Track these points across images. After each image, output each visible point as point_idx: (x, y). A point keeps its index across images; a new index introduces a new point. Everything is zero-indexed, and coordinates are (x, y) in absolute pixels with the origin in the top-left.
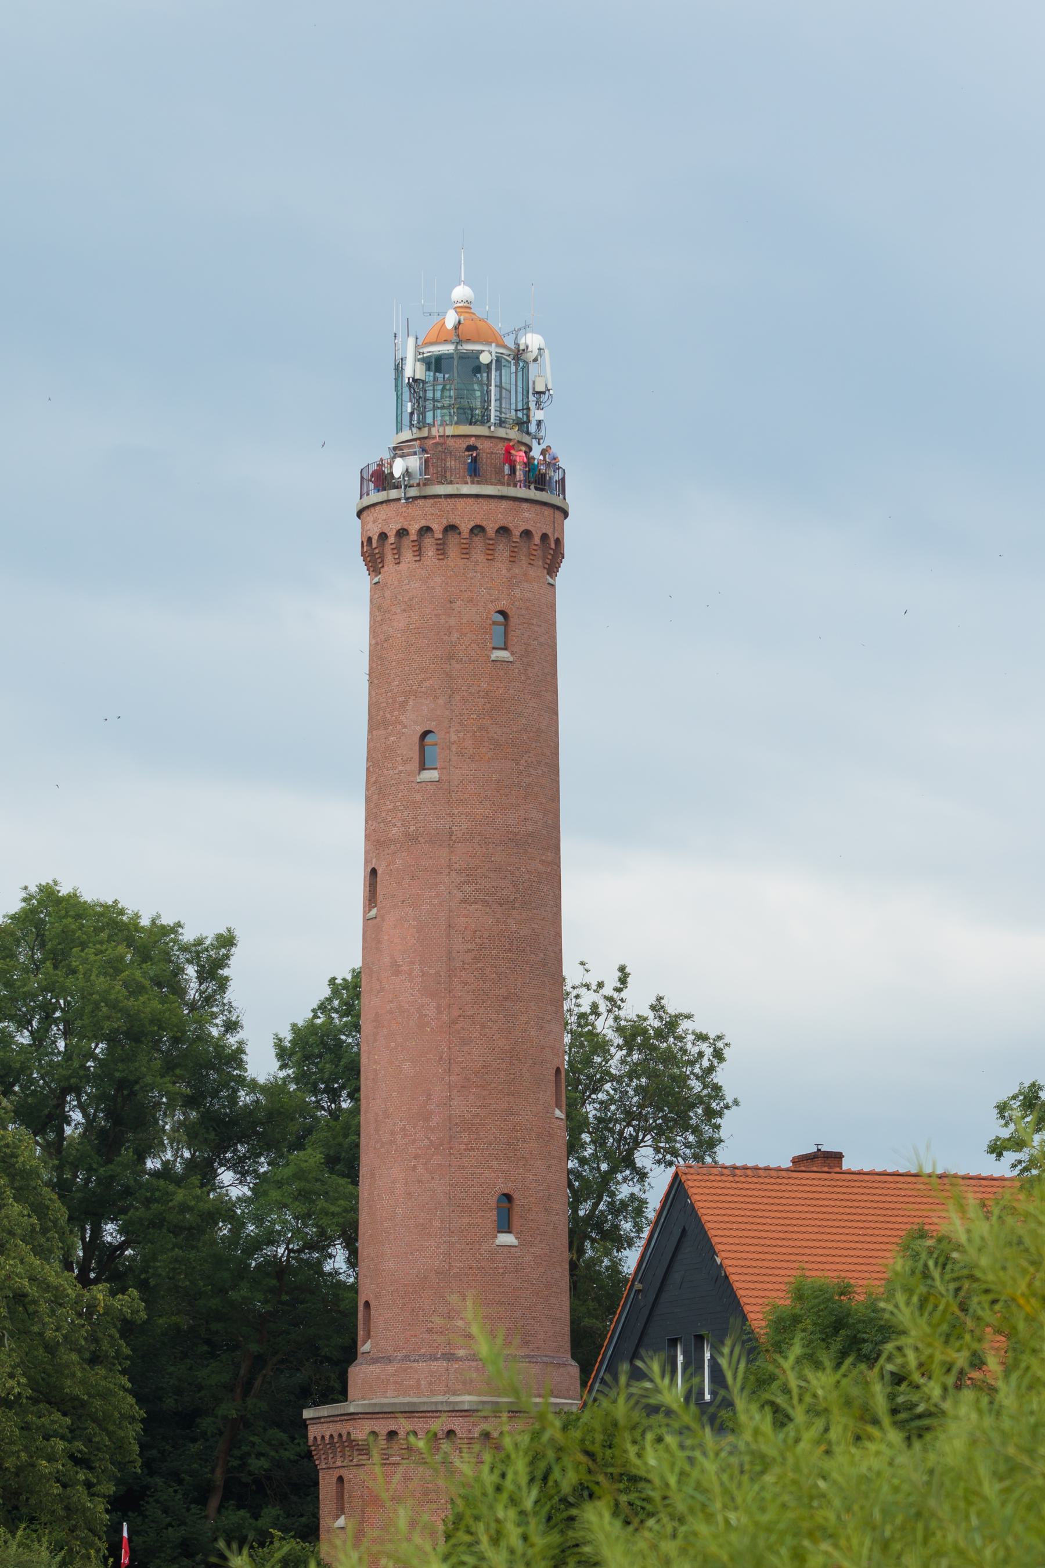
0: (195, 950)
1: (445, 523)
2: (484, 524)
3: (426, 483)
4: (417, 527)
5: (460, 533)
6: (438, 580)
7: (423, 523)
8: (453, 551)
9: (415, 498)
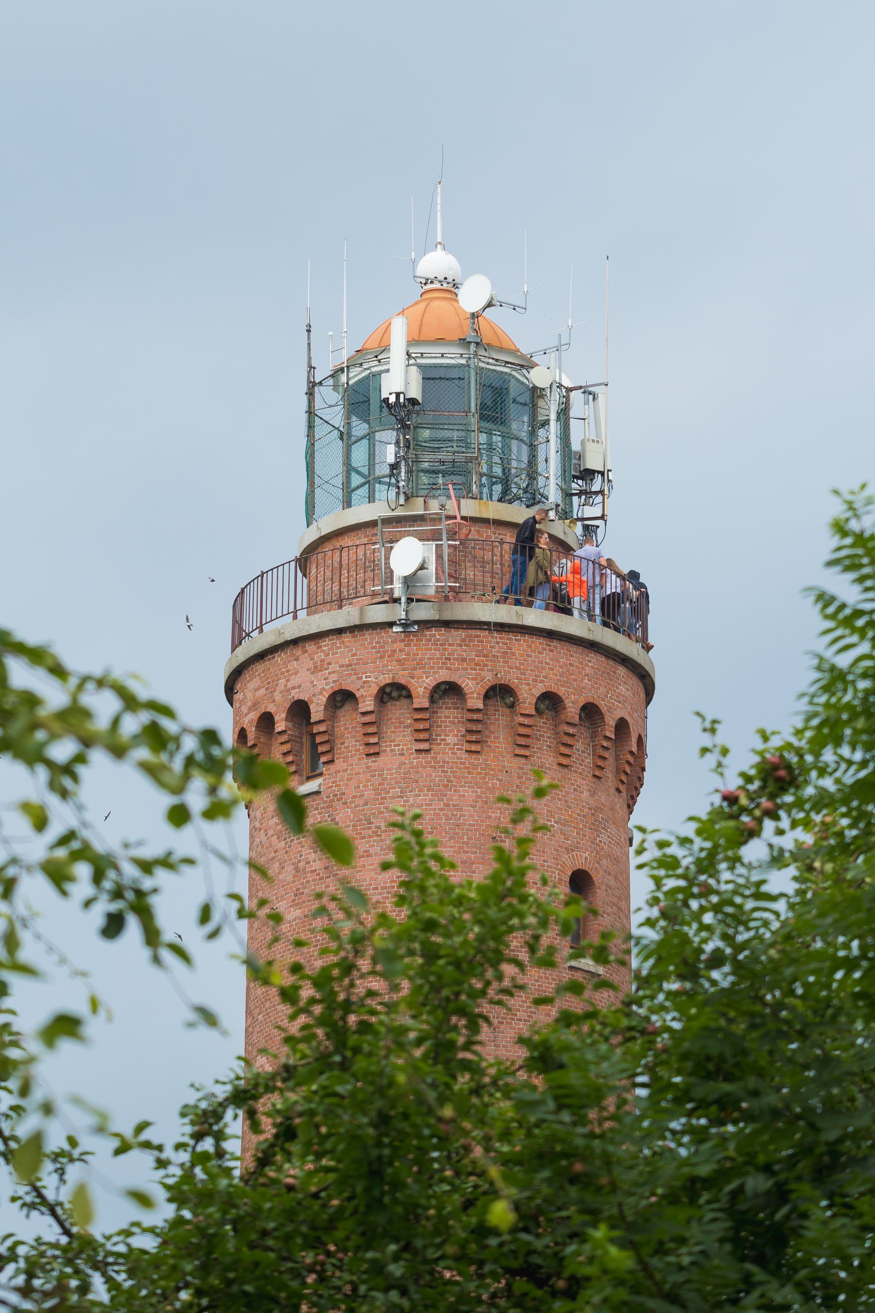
0: (540, 389)
1: (489, 679)
2: (561, 691)
3: (456, 594)
4: (430, 682)
5: (512, 706)
6: (469, 793)
7: (443, 675)
8: (500, 739)
9: (425, 624)
